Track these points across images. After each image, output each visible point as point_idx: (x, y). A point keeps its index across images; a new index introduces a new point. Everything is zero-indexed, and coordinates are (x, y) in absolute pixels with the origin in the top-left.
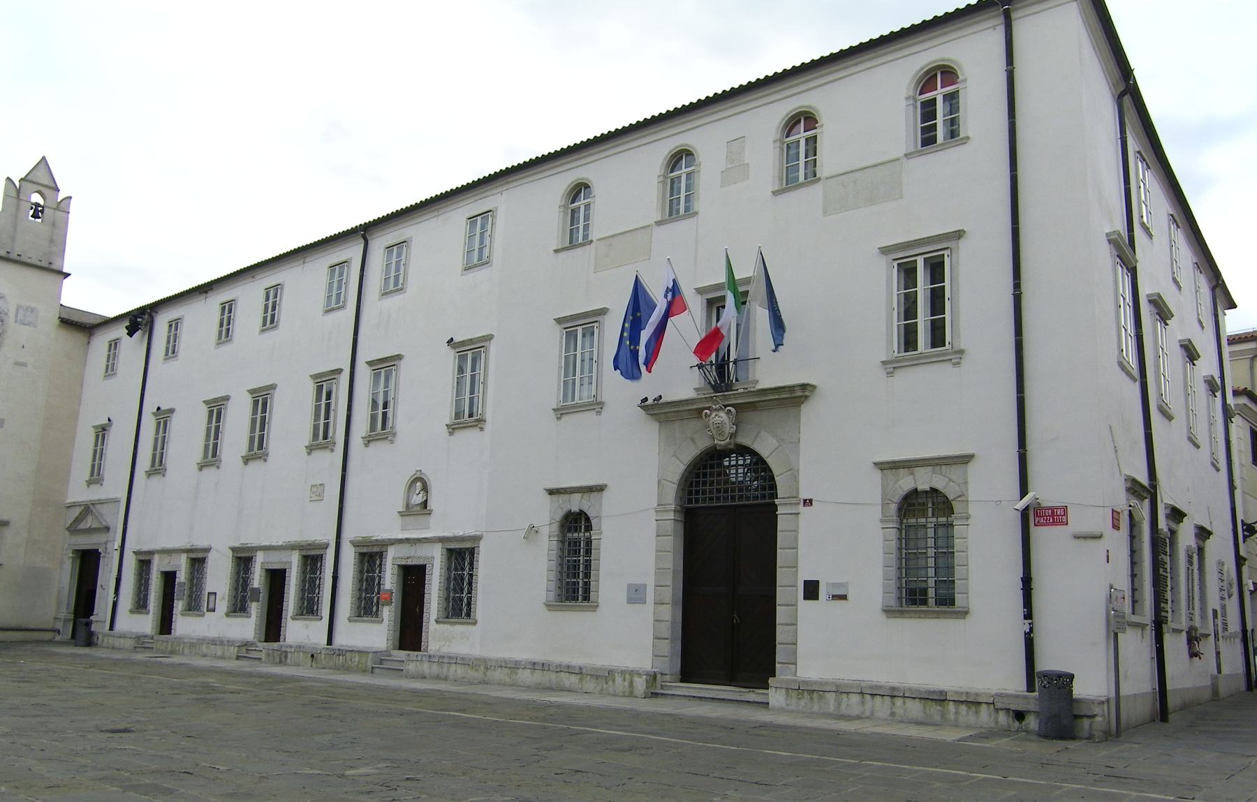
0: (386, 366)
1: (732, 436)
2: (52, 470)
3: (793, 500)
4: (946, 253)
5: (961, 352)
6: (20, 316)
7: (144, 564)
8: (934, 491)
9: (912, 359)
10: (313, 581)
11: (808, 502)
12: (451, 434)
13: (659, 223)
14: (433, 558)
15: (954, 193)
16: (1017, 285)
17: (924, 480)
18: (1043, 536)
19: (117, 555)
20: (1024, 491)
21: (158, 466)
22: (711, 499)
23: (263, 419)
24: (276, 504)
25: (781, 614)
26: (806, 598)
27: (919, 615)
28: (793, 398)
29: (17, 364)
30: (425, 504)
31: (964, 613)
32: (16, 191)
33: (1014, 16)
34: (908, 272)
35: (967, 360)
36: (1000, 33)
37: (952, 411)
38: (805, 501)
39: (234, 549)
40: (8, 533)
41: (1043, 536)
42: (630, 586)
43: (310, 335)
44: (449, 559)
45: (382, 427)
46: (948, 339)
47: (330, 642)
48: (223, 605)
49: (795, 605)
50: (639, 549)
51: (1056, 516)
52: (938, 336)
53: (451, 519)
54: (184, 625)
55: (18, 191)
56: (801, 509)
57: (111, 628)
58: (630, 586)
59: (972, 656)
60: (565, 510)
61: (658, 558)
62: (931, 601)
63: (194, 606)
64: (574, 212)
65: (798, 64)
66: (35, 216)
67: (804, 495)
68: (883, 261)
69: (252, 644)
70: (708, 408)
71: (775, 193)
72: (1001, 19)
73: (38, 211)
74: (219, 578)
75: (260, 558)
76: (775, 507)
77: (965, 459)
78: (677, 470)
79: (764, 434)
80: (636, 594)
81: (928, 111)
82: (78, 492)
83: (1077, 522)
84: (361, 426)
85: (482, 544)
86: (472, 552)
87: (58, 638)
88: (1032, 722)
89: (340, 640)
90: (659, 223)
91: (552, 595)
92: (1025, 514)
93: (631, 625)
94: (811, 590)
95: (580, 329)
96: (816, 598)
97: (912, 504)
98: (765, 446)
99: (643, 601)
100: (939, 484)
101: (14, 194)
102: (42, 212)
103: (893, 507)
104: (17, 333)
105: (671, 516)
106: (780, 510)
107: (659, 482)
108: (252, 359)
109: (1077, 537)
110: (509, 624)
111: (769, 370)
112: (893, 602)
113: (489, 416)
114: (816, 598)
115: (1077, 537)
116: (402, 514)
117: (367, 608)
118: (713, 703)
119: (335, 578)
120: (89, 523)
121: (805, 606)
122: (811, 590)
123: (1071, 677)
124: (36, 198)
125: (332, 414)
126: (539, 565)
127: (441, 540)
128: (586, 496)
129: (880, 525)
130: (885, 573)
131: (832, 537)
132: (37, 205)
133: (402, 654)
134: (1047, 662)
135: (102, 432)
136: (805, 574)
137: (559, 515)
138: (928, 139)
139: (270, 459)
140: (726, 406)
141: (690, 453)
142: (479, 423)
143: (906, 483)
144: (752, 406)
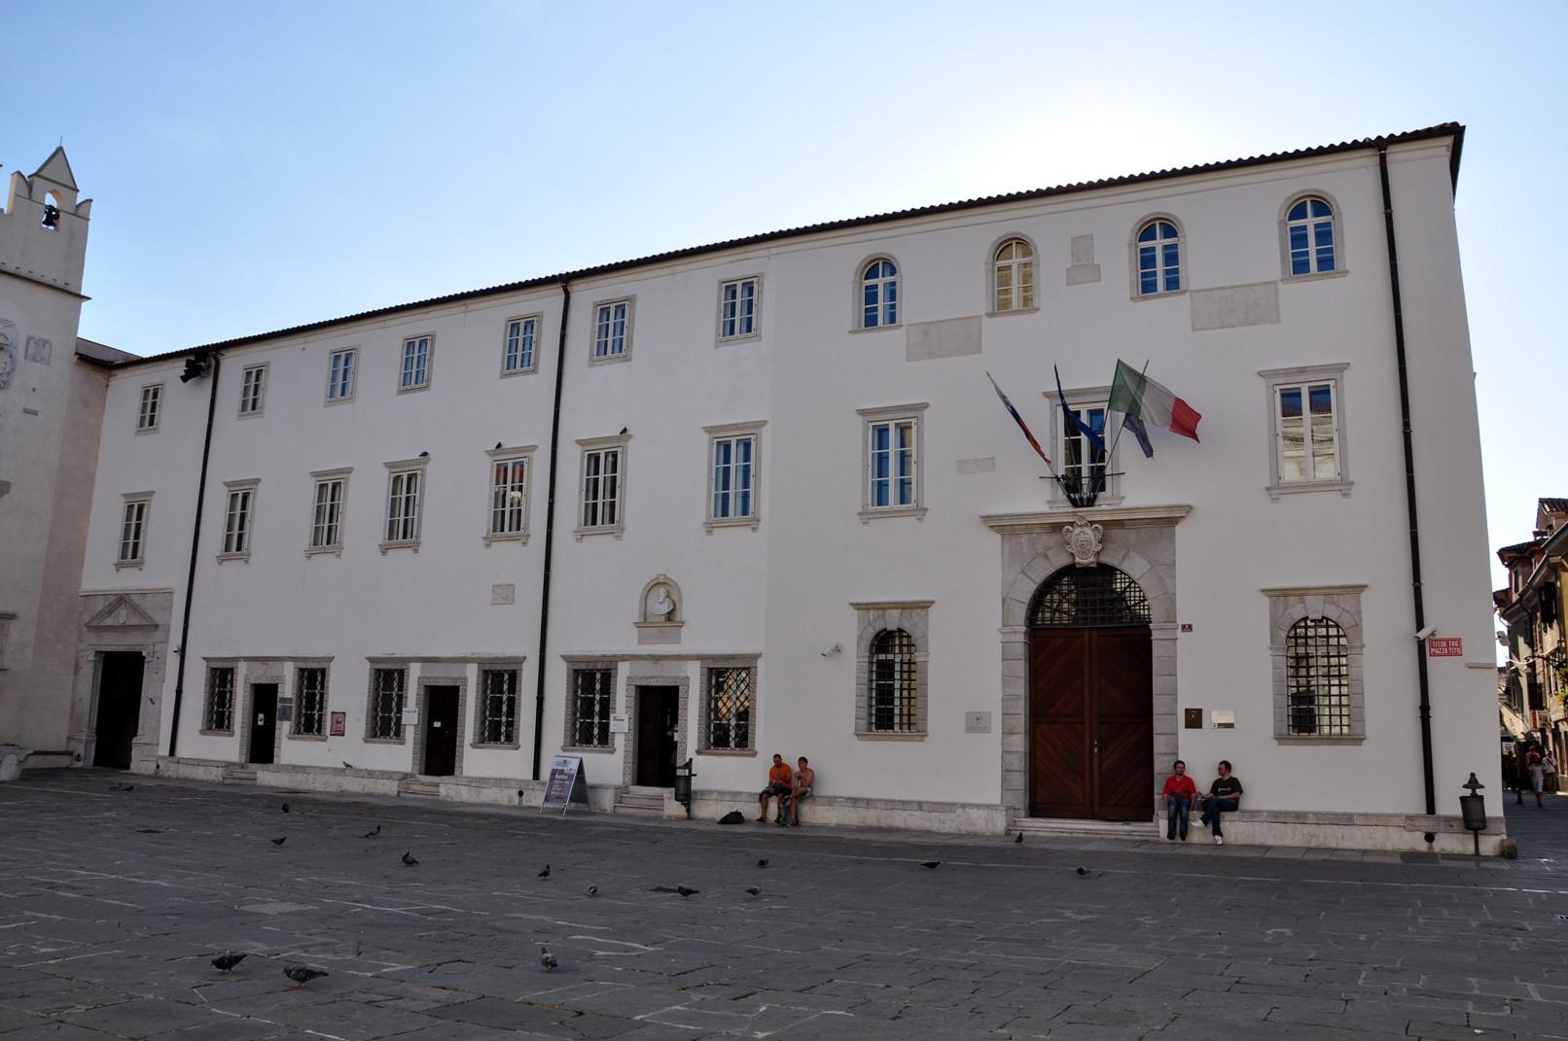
2: (64, 555)
6: (31, 351)
7: (221, 678)
10: (222, 695)
12: (488, 546)
14: (465, 679)
16: (1406, 424)
17: (1315, 608)
19: (173, 662)
21: (236, 542)
23: (138, 526)
24: (453, 607)
28: (1167, 522)
29: (26, 411)
32: (27, 186)
33: (1389, 159)
40: (14, 627)
42: (968, 714)
43: (481, 410)
50: (976, 671)
51: (1453, 647)
53: (708, 633)
54: (290, 748)
55: (30, 187)
57: (172, 752)
58: (968, 714)
60: (878, 628)
63: (310, 724)
66: (48, 222)
67: (1180, 621)
68: (1261, 384)
69: (412, 775)
73: (52, 217)
74: (349, 695)
75: (415, 673)
78: (1027, 589)
80: (976, 723)
81: (871, 296)
82: (101, 574)
86: (323, 672)
87: (79, 764)
89: (182, 751)
91: (864, 723)
93: (963, 767)
99: (986, 730)
100: (1333, 613)
101: (25, 192)
102: (57, 216)
104: (28, 373)
106: (1155, 635)
108: (371, 435)
117: (218, 719)
119: (540, 699)
120: (122, 617)
121: (1186, 736)
122: (1194, 719)
124: (50, 200)
125: (752, 480)
126: (846, 684)
127: (698, 657)
128: (907, 613)
132: (51, 208)
133: (254, 767)
135: (136, 511)
137: (871, 633)
138: (871, 321)
141: (1043, 571)
144: (1119, 524)
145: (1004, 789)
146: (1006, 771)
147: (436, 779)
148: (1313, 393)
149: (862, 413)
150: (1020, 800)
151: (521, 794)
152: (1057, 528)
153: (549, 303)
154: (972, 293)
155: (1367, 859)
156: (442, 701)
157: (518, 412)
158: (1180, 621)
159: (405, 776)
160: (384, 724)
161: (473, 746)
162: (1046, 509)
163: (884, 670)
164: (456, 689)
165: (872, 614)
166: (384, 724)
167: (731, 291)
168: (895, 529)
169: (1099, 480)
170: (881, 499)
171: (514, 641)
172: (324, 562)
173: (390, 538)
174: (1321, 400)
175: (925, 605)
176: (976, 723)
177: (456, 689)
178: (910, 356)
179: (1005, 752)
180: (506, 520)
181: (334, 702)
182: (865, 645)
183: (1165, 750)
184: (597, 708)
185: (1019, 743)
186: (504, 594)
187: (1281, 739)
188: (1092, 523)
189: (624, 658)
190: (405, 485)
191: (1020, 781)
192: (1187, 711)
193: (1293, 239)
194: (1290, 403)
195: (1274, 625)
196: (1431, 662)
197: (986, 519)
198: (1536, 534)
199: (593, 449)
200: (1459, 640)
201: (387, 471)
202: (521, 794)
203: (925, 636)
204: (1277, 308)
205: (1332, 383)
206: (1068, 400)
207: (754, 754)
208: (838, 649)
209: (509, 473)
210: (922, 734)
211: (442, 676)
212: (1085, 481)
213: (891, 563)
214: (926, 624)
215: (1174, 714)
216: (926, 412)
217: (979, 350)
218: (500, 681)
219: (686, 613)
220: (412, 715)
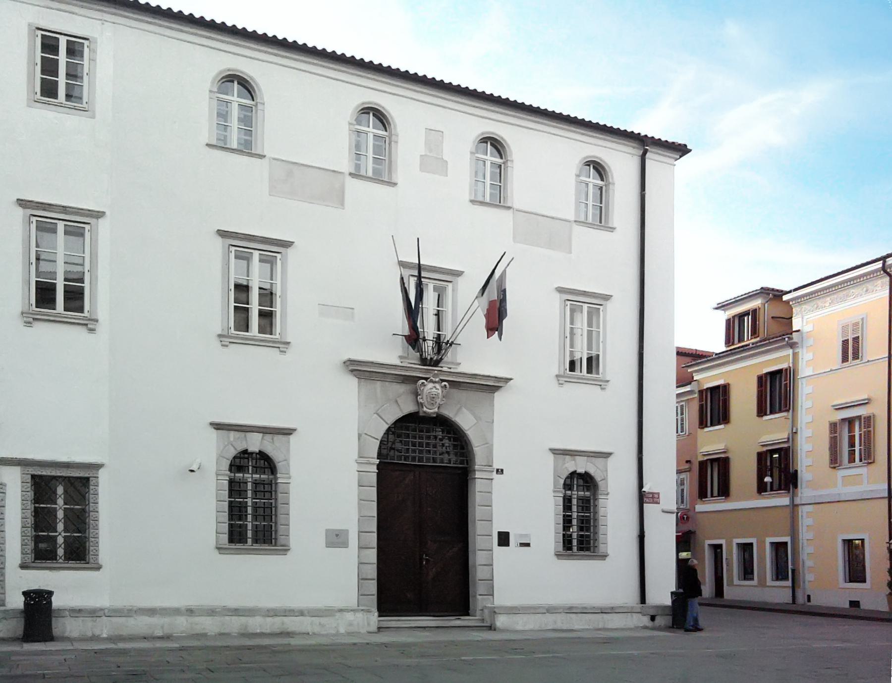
3: (489, 469)
4: (279, 256)
8: (261, 453)
9: (242, 338)
11: (500, 471)
13: (350, 174)
22: (414, 459)
26: (499, 545)
27: (239, 552)
28: (490, 386)
31: (604, 557)
35: (291, 352)
38: (497, 470)
42: (327, 531)
46: (87, 307)
47: (643, 599)
49: (491, 550)
50: (332, 491)
58: (327, 531)
59: (602, 585)
60: (571, 470)
62: (575, 549)
65: (479, 90)
67: (496, 466)
70: (426, 379)
77: (607, 455)
80: (336, 539)
85: (102, 474)
89: (729, 593)
93: (323, 568)
94: (504, 539)
95: (585, 306)
96: (507, 544)
97: (242, 461)
98: (465, 420)
99: (345, 545)
105: (478, 475)
107: (360, 436)
110: (156, 564)
114: (507, 544)
118: (417, 630)
121: (499, 552)
122: (504, 539)
123: (50, 593)
128: (268, 437)
129: (553, 494)
130: (556, 529)
131: (514, 498)
136: (499, 526)
137: (232, 453)
141: (393, 414)
146: (361, 579)
152: (412, 380)
162: (397, 362)
165: (232, 434)
167: (49, 45)
170: (243, 323)
174: (45, 294)
175: (287, 432)
176: (336, 539)
179: (360, 563)
182: (226, 465)
188: (443, 381)
192: (500, 533)
194: (75, 297)
195: (556, 476)
198: (401, 357)
200: (658, 494)
203: (605, 479)
206: (423, 274)
210: (285, 550)
213: (257, 389)
214: (288, 450)
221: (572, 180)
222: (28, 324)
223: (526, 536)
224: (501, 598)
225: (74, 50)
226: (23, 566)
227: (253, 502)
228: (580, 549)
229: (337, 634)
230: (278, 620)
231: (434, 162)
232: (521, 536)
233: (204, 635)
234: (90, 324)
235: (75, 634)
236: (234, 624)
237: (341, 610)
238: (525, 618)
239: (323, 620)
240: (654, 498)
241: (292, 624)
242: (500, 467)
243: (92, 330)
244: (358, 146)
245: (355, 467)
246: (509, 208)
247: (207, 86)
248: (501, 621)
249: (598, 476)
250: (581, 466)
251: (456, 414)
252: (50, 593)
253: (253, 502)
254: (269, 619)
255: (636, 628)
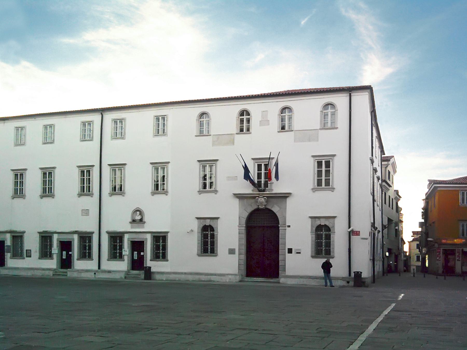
0: (118, 168)
1: (265, 205)
4: (331, 160)
5: (334, 188)
8: (325, 225)
11: (289, 226)
13: (237, 134)
15: (331, 143)
17: (323, 222)
18: (354, 238)
20: (349, 227)
25: (281, 257)
26: (288, 253)
28: (285, 196)
30: (141, 220)
33: (352, 94)
34: (320, 164)
35: (335, 191)
36: (348, 98)
37: (330, 204)
39: (39, 233)
41: (354, 238)
44: (42, 239)
45: (118, 190)
48: (36, 253)
50: (231, 235)
51: (357, 233)
52: (327, 183)
53: (154, 224)
56: (287, 228)
61: (239, 241)
64: (326, 115)
67: (287, 224)
71: (278, 132)
72: (348, 95)
74: (32, 243)
75: (55, 237)
76: (279, 227)
78: (246, 215)
79: (275, 206)
80: (232, 252)
83: (362, 235)
84: (107, 188)
85: (169, 234)
88: (352, 283)
89: (103, 267)
90: (237, 134)
91: (200, 252)
92: (350, 232)
93: (228, 263)
94: (290, 251)
97: (319, 228)
98: (275, 209)
100: (327, 223)
103: (314, 229)
105: (244, 228)
107: (239, 218)
109: (362, 239)
110: (183, 260)
111: (277, 187)
112: (314, 254)
113: (169, 190)
115: (362, 239)
116: (130, 223)
118: (259, 282)
121: (288, 255)
123: (361, 273)
125: (165, 180)
126: (194, 242)
128: (212, 220)
131: (296, 235)
134: (355, 269)
136: (288, 246)
137: (202, 226)
139: (56, 197)
140: (264, 197)
141: (250, 210)
142: (165, 192)
143: (318, 222)
145: (239, 269)
146: (239, 265)
147: (65, 270)
148: (326, 162)
149: (313, 156)
150: (244, 273)
151: (95, 274)
152: (254, 198)
153: (96, 118)
154: (232, 125)
155: (194, 282)
156: (66, 246)
157: (88, 154)
158: (287, 224)
159: (55, 269)
160: (45, 253)
161: (78, 260)
162: (251, 192)
163: (205, 237)
164: (71, 242)
165: (202, 220)
166: (115, 254)
167: (158, 119)
168: (324, 195)
169: (266, 185)
171: (88, 225)
172: (46, 200)
173: (15, 194)
176: (232, 252)
177: (71, 242)
178: (213, 145)
179: (239, 259)
180: (85, 190)
181: (26, 247)
183: (282, 259)
184: (87, 248)
185: (243, 257)
186: (86, 212)
187: (313, 257)
188: (264, 197)
189: (56, 233)
190: (48, 175)
191: (244, 267)
192: (288, 249)
193: (240, 121)
195: (312, 226)
196: (352, 236)
197: (235, 194)
199: (260, 162)
201: (77, 169)
202: (95, 274)
203: (217, 227)
204: (318, 137)
205: (331, 160)
207: (167, 261)
208: (192, 231)
209: (85, 172)
211: (65, 238)
212: (262, 185)
213: (208, 206)
214: (217, 224)
215: (285, 249)
216: (218, 162)
217: (318, 141)
218: (85, 238)
219: (146, 219)
220: (55, 249)
221: (319, 113)
222: (153, 195)
223: (300, 250)
224: (289, 272)
225: (164, 119)
226: (151, 260)
227: (208, 240)
228: (211, 253)
229: (226, 282)
230: (209, 277)
231: (264, 122)
232: (297, 250)
233: (189, 280)
234: (333, 189)
235: (158, 279)
236: (197, 277)
237: (228, 275)
238: (291, 279)
239: (222, 277)
240: (357, 233)
241: (213, 278)
242: (289, 225)
243: (167, 195)
244: (208, 126)
245: (238, 228)
246: (293, 131)
247: (196, 118)
248: (158, 277)
249: (330, 226)
250: (208, 223)
251: (272, 207)
252: (361, 273)
253: (208, 240)
254: (206, 276)
255: (320, 285)
